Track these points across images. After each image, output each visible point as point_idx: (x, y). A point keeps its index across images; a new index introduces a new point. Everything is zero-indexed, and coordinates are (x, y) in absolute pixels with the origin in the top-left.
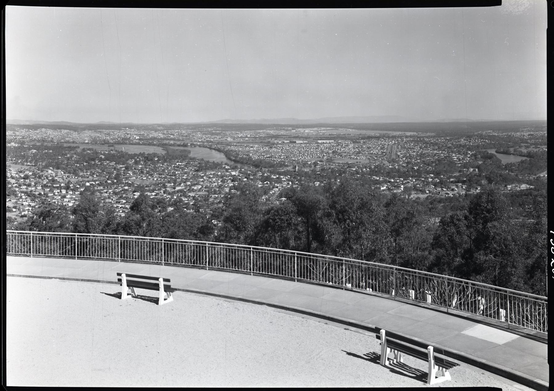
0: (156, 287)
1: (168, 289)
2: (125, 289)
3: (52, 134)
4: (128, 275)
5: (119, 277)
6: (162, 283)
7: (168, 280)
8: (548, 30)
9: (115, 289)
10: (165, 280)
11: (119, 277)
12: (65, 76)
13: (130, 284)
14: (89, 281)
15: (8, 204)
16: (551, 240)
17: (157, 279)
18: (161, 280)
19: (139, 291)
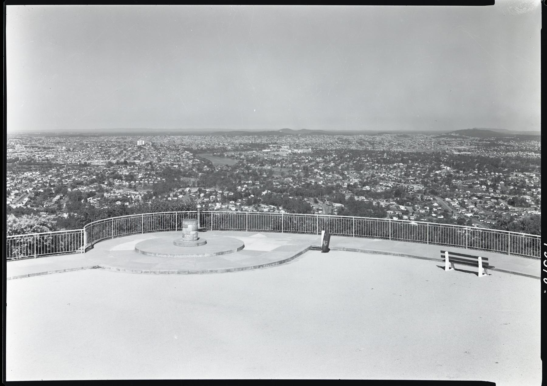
0: (476, 264)
1: (485, 266)
2: (447, 264)
3: (199, 140)
4: (450, 253)
5: (443, 254)
6: (480, 261)
7: (487, 259)
8: (542, 31)
9: (442, 264)
10: (483, 258)
11: (443, 254)
12: (63, 86)
13: (452, 260)
14: (39, 274)
15: (540, 196)
16: (545, 253)
17: (477, 257)
18: (480, 258)
19: (457, 266)
